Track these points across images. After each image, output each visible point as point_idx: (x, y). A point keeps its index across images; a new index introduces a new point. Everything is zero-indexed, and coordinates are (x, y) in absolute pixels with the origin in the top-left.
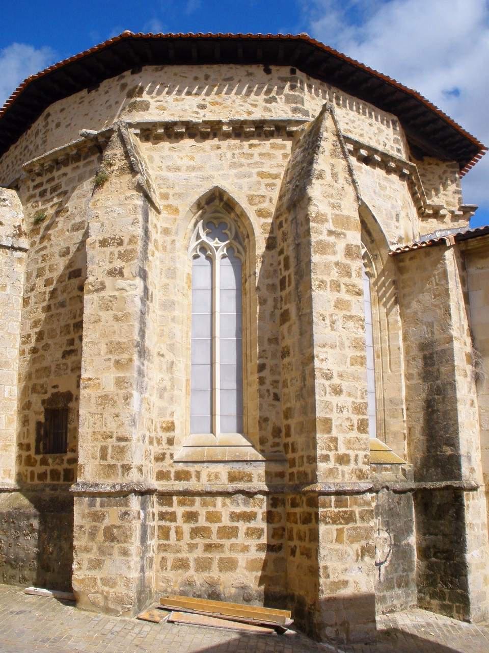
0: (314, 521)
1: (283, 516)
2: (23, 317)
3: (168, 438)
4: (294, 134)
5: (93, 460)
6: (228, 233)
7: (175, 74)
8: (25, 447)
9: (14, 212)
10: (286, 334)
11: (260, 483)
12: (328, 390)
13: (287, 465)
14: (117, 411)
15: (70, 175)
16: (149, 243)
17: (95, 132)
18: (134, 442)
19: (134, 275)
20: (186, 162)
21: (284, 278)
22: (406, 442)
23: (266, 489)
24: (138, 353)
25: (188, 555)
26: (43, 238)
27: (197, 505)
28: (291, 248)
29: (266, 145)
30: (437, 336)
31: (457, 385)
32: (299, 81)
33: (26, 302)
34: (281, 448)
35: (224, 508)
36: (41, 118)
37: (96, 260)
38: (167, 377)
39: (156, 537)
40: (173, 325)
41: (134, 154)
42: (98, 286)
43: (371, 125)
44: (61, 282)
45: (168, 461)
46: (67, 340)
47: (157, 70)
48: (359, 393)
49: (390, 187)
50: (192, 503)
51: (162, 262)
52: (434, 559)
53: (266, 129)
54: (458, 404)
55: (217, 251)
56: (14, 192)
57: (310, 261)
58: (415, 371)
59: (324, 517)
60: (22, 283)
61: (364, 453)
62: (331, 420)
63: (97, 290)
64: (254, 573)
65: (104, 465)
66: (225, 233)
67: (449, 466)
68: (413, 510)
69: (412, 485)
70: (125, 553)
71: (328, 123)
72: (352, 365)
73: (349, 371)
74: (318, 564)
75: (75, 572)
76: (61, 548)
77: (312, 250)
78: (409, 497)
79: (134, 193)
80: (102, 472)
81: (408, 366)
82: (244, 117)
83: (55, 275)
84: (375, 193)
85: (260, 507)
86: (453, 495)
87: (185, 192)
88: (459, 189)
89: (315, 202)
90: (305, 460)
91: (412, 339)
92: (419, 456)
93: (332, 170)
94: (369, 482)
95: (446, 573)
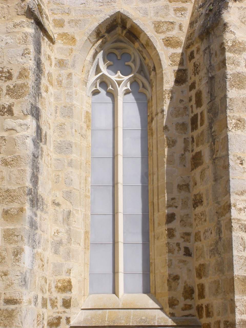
3: (63, 299)
16: (42, 77)
18: (24, 305)
19: (26, 113)
21: (196, 116)
24: (29, 202)
28: (204, 82)
34: (193, 311)
40: (70, 169)
51: (57, 98)
57: (225, 97)
66: (129, 66)
77: (228, 83)
79: (24, 19)
87: (82, 18)
89: (232, 28)
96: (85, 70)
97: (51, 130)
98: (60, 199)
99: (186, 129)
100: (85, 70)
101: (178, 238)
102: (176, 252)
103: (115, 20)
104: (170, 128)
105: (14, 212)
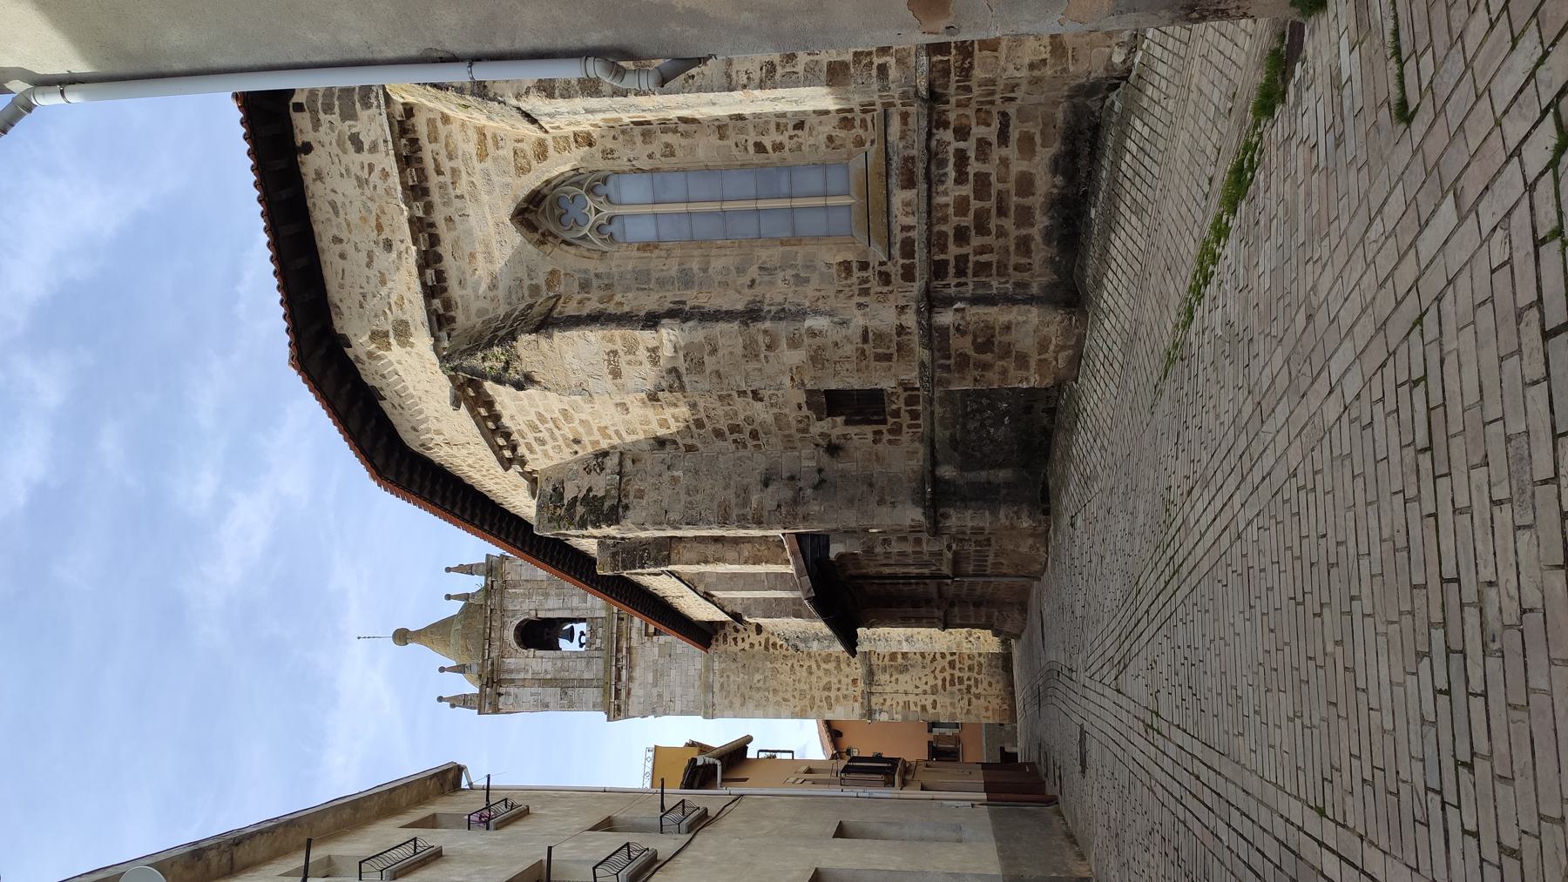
4: (408, 107)
8: (878, 437)
13: (892, 110)
34: (868, 117)
38: (781, 275)
45: (889, 268)
50: (943, 235)
51: (627, 289)
59: (962, 71)
62: (830, 64)
63: (679, 377)
64: (1037, 149)
70: (1007, 328)
96: (586, 254)
99: (649, 131)
100: (586, 254)
102: (800, 140)
103: (521, 223)
104: (650, 152)
105: (767, 340)
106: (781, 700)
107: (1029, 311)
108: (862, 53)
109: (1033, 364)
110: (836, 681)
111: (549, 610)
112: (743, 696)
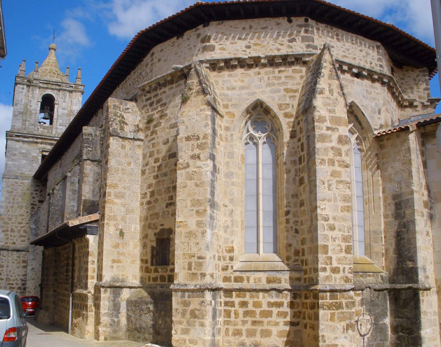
0: (316, 307)
1: (300, 304)
2: (142, 182)
3: (230, 256)
5: (183, 270)
6: (267, 128)
7: (231, 26)
8: (144, 261)
9: (134, 116)
10: (302, 191)
11: (286, 284)
12: (326, 227)
13: (303, 273)
14: (197, 241)
15: (167, 93)
16: (216, 137)
17: (181, 66)
18: (207, 260)
19: (207, 158)
20: (240, 84)
21: (301, 157)
22: (384, 259)
23: (290, 288)
24: (209, 206)
25: (242, 327)
26: (153, 133)
27: (248, 297)
28: (305, 138)
29: (289, 71)
30: (404, 190)
31: (416, 222)
32: (310, 26)
33: (143, 172)
34: (299, 263)
35: (264, 299)
36: (149, 55)
37: (184, 149)
39: (222, 316)
40: (233, 187)
41: (205, 82)
42: (185, 165)
43: (361, 51)
44: (164, 161)
45: (230, 271)
46: (169, 197)
47: (219, 24)
48: (346, 229)
49: (374, 92)
50: (245, 296)
51: (225, 148)
52: (401, 334)
53: (289, 60)
54: (417, 235)
55: (260, 139)
56: (133, 103)
57: (315, 147)
58: (390, 213)
60: (141, 161)
61: (349, 266)
62: (327, 246)
63: (184, 168)
65: (190, 273)
66: (265, 128)
67: (410, 274)
68: (388, 302)
69: (388, 286)
70: (202, 325)
71: (327, 57)
72: (342, 211)
73: (340, 215)
74: (318, 334)
75: (174, 336)
76: (166, 322)
77: (316, 140)
78: (385, 294)
79: (205, 107)
80: (189, 277)
81: (385, 209)
82: (276, 53)
83: (160, 156)
84: (363, 96)
85: (286, 299)
86: (413, 293)
87: (238, 103)
88: (428, 87)
89: (318, 109)
90: (312, 270)
91: (388, 192)
92: (392, 267)
93: (329, 87)
94: (352, 284)
95: (408, 342)
97: (222, 166)
98: (227, 203)
99: (296, 164)
101: (291, 224)
102: (290, 231)
103: (257, 104)
104: (287, 163)
105: (201, 211)
106: (8, 209)
107: (210, 335)
108: (331, 260)
109: (184, 336)
110: (15, 235)
111: (58, 110)
112: (12, 192)
